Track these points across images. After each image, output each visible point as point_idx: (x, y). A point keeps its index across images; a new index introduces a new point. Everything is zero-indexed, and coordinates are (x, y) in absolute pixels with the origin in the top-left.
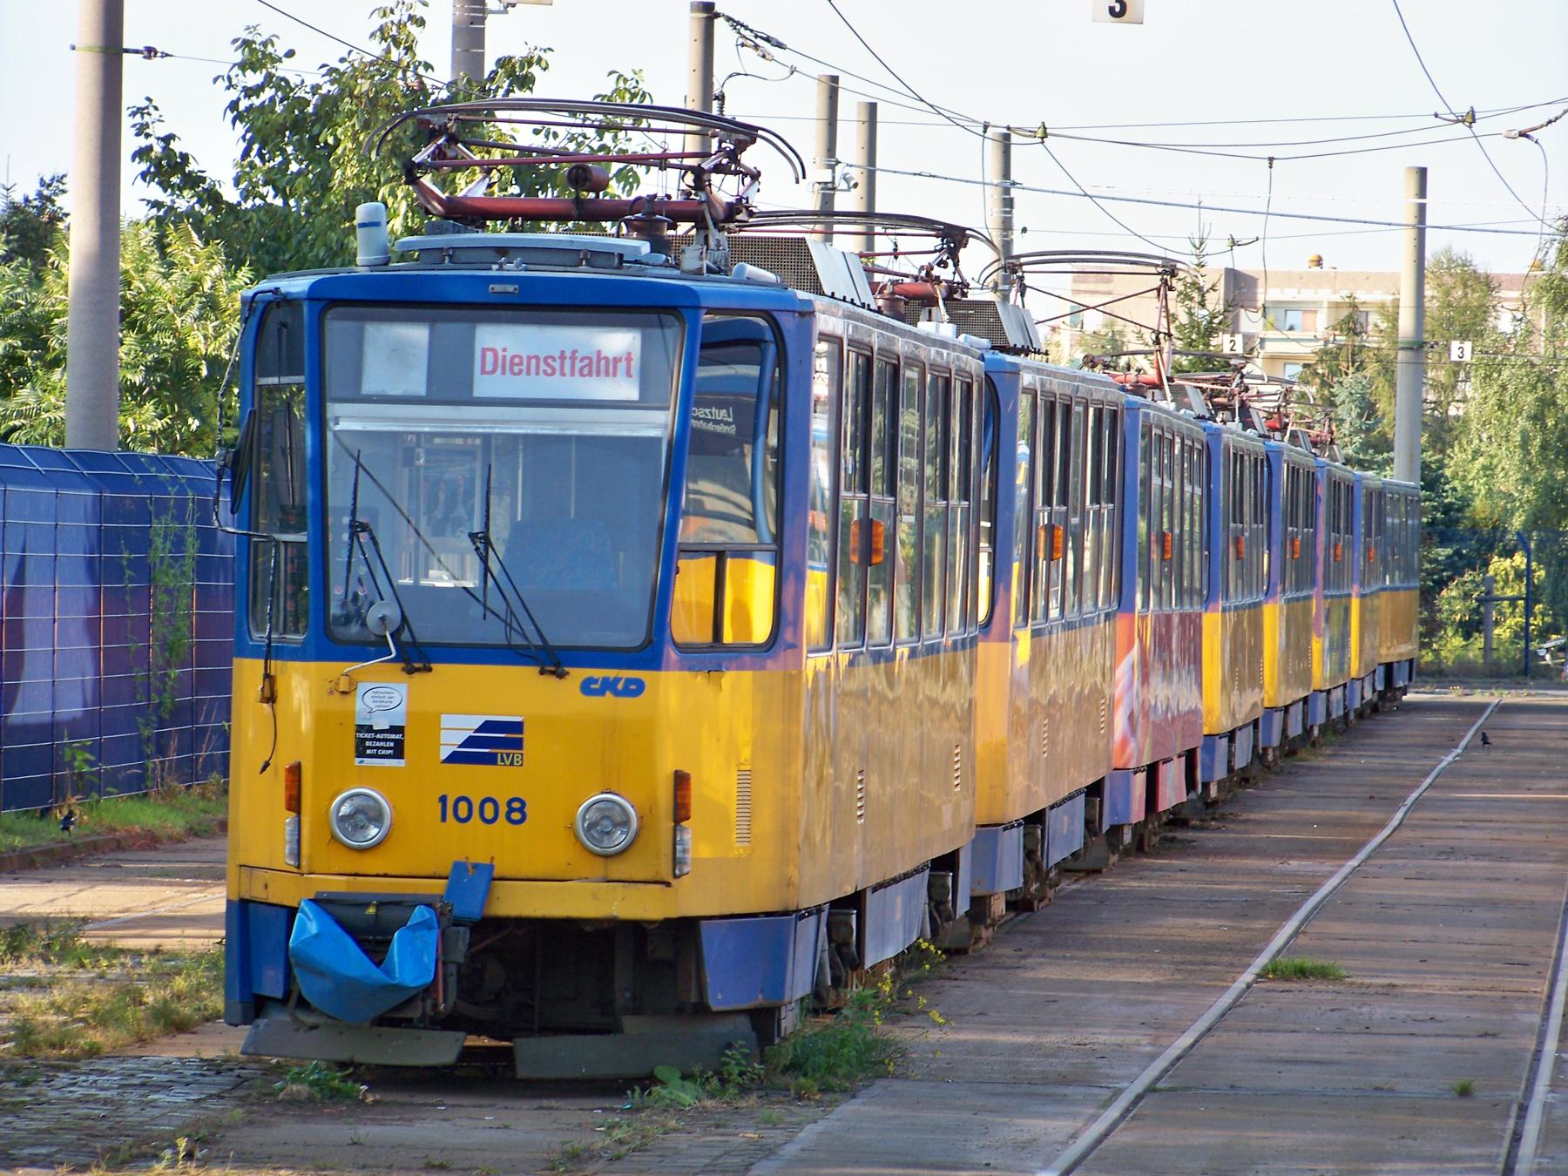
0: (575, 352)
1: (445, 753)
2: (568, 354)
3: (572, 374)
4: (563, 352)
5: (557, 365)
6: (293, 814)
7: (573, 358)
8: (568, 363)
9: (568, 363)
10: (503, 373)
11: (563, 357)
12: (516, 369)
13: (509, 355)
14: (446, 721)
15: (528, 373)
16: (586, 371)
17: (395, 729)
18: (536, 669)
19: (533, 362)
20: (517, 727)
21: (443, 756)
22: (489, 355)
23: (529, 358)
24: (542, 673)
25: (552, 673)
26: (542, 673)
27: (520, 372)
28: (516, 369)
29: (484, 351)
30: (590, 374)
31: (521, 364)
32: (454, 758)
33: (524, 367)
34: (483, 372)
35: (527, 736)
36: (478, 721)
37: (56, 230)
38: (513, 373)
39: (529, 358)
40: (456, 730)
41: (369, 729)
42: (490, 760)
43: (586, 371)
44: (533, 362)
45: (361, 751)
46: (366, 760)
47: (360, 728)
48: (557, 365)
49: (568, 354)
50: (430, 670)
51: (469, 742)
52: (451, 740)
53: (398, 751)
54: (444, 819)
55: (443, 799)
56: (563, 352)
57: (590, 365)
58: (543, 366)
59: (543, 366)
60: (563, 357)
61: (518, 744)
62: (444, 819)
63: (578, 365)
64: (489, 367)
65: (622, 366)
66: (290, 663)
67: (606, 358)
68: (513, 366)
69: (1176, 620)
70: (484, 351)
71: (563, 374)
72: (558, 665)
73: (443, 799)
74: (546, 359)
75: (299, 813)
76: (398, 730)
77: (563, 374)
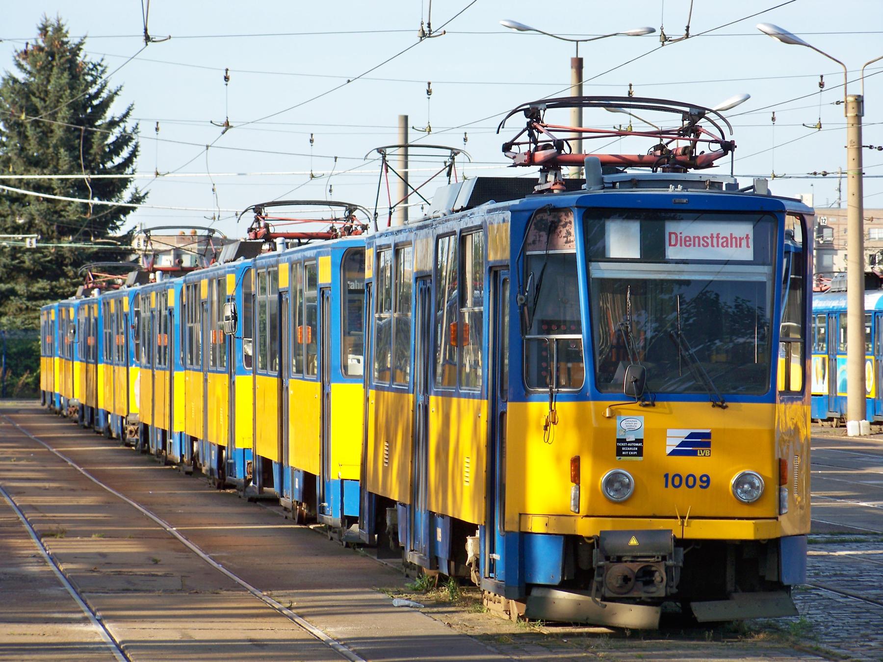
0: (718, 234)
1: (669, 450)
2: (715, 235)
3: (718, 246)
4: (712, 235)
5: (709, 241)
6: (574, 484)
7: (718, 237)
8: (715, 240)
9: (715, 240)
10: (681, 245)
11: (712, 237)
12: (688, 243)
13: (683, 236)
14: (670, 432)
15: (694, 246)
16: (725, 244)
17: (637, 441)
18: (711, 404)
19: (697, 240)
20: (708, 435)
21: (668, 452)
22: (673, 236)
23: (694, 238)
24: (713, 406)
25: (720, 406)
26: (713, 406)
27: (690, 245)
28: (688, 243)
29: (670, 234)
30: (727, 246)
31: (690, 240)
32: (674, 453)
33: (692, 243)
34: (670, 245)
35: (713, 440)
36: (687, 433)
37: (77, 65)
38: (686, 245)
39: (694, 238)
40: (674, 438)
41: (624, 441)
42: (694, 453)
43: (725, 244)
44: (697, 240)
45: (619, 452)
46: (623, 458)
47: (619, 441)
48: (709, 241)
49: (715, 235)
50: (654, 405)
51: (682, 444)
52: (672, 444)
53: (640, 452)
54: (666, 486)
55: (666, 476)
56: (712, 235)
57: (727, 241)
58: (702, 242)
59: (702, 242)
60: (712, 237)
61: (708, 445)
62: (666, 486)
63: (721, 241)
64: (673, 243)
65: (744, 242)
66: (672, 403)
67: (736, 238)
68: (688, 242)
69: (852, 322)
70: (670, 234)
71: (713, 246)
72: (723, 402)
73: (666, 476)
74: (703, 238)
75: (578, 484)
76: (641, 441)
77: (713, 246)
